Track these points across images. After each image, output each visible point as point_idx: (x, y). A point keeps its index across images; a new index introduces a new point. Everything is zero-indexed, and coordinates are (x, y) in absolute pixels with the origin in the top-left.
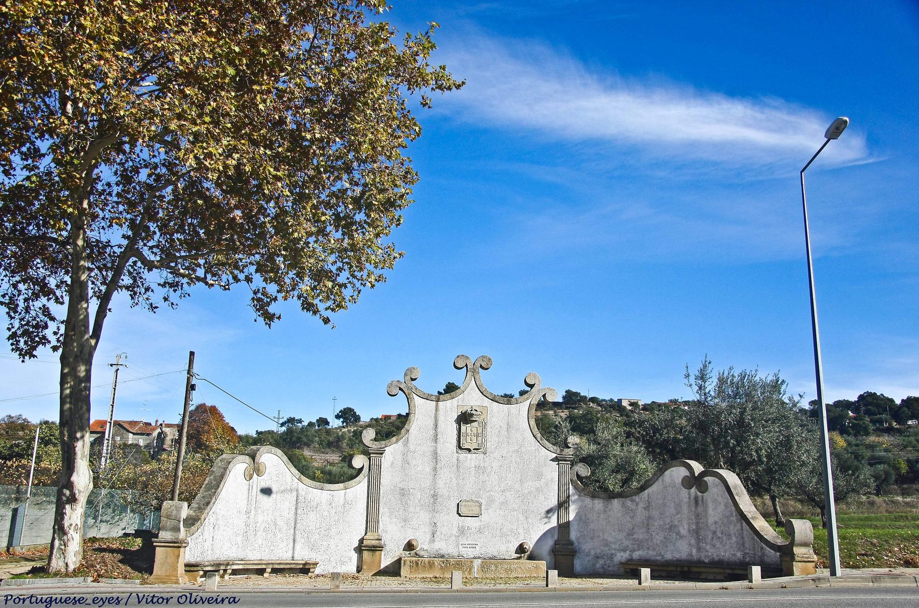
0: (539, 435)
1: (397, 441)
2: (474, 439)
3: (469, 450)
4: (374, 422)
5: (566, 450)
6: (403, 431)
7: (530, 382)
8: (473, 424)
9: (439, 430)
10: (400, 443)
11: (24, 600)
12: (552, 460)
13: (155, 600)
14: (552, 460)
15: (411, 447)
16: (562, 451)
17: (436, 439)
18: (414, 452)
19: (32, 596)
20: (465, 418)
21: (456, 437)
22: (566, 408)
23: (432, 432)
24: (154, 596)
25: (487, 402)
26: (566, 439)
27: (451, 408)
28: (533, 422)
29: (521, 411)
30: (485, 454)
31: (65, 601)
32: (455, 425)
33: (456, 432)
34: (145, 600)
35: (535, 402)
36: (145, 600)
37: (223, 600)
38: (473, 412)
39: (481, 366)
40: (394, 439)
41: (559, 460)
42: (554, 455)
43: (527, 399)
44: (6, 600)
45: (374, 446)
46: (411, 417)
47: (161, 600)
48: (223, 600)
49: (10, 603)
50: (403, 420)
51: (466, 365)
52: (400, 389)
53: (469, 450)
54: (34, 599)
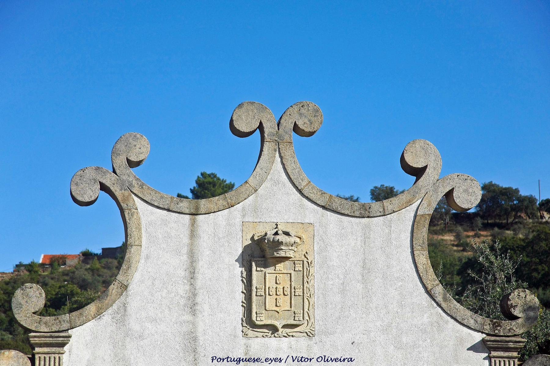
0: (439, 290)
1: (99, 314)
2: (284, 302)
3: (274, 329)
4: (24, 273)
5: (507, 324)
6: (113, 288)
7: (415, 162)
8: (280, 266)
9: (199, 283)
10: (107, 317)
11: (223, 360)
12: (474, 348)
13: (303, 359)
14: (474, 348)
15: (134, 325)
16: (495, 326)
17: (193, 307)
18: (141, 337)
19: (228, 357)
20: (261, 253)
21: (241, 297)
22: (486, 226)
23: (182, 289)
24: (302, 357)
25: (312, 213)
26: (506, 298)
27: (226, 230)
28: (423, 259)
29: (395, 234)
30: (309, 335)
31: (248, 360)
32: (238, 270)
33: (240, 287)
34: (296, 360)
35: (428, 210)
36: (296, 360)
37: (344, 360)
38: (281, 238)
39: (296, 128)
40: (91, 308)
41: (490, 349)
42: (478, 337)
43: (409, 203)
44: (213, 360)
45: (41, 327)
46: (132, 252)
47: (306, 360)
48: (344, 360)
49: (215, 361)
50: (115, 259)
51: (261, 127)
52: (104, 187)
53: (274, 329)
54: (229, 359)
